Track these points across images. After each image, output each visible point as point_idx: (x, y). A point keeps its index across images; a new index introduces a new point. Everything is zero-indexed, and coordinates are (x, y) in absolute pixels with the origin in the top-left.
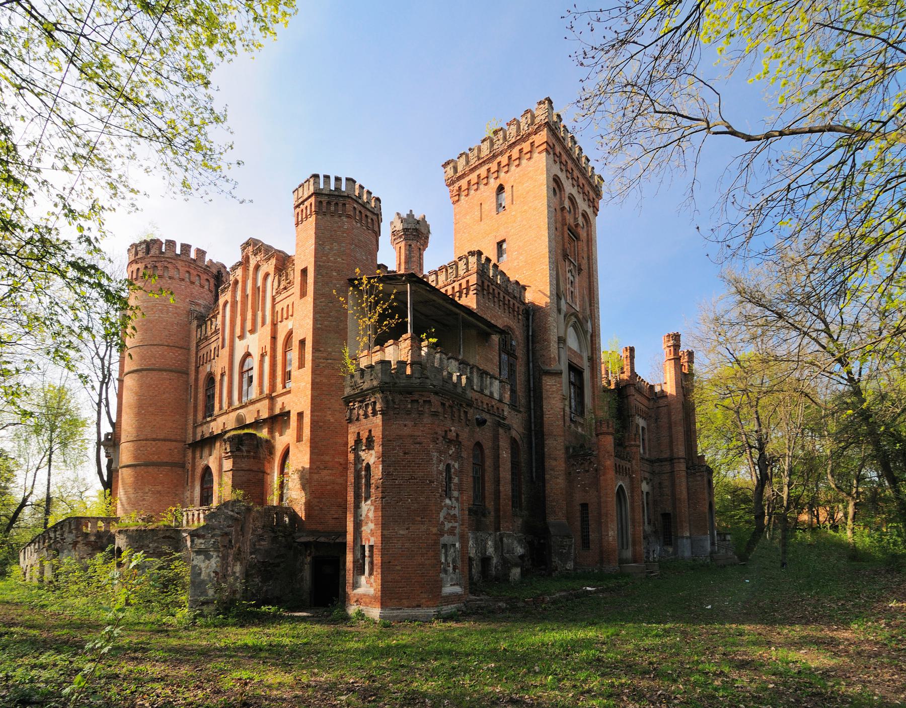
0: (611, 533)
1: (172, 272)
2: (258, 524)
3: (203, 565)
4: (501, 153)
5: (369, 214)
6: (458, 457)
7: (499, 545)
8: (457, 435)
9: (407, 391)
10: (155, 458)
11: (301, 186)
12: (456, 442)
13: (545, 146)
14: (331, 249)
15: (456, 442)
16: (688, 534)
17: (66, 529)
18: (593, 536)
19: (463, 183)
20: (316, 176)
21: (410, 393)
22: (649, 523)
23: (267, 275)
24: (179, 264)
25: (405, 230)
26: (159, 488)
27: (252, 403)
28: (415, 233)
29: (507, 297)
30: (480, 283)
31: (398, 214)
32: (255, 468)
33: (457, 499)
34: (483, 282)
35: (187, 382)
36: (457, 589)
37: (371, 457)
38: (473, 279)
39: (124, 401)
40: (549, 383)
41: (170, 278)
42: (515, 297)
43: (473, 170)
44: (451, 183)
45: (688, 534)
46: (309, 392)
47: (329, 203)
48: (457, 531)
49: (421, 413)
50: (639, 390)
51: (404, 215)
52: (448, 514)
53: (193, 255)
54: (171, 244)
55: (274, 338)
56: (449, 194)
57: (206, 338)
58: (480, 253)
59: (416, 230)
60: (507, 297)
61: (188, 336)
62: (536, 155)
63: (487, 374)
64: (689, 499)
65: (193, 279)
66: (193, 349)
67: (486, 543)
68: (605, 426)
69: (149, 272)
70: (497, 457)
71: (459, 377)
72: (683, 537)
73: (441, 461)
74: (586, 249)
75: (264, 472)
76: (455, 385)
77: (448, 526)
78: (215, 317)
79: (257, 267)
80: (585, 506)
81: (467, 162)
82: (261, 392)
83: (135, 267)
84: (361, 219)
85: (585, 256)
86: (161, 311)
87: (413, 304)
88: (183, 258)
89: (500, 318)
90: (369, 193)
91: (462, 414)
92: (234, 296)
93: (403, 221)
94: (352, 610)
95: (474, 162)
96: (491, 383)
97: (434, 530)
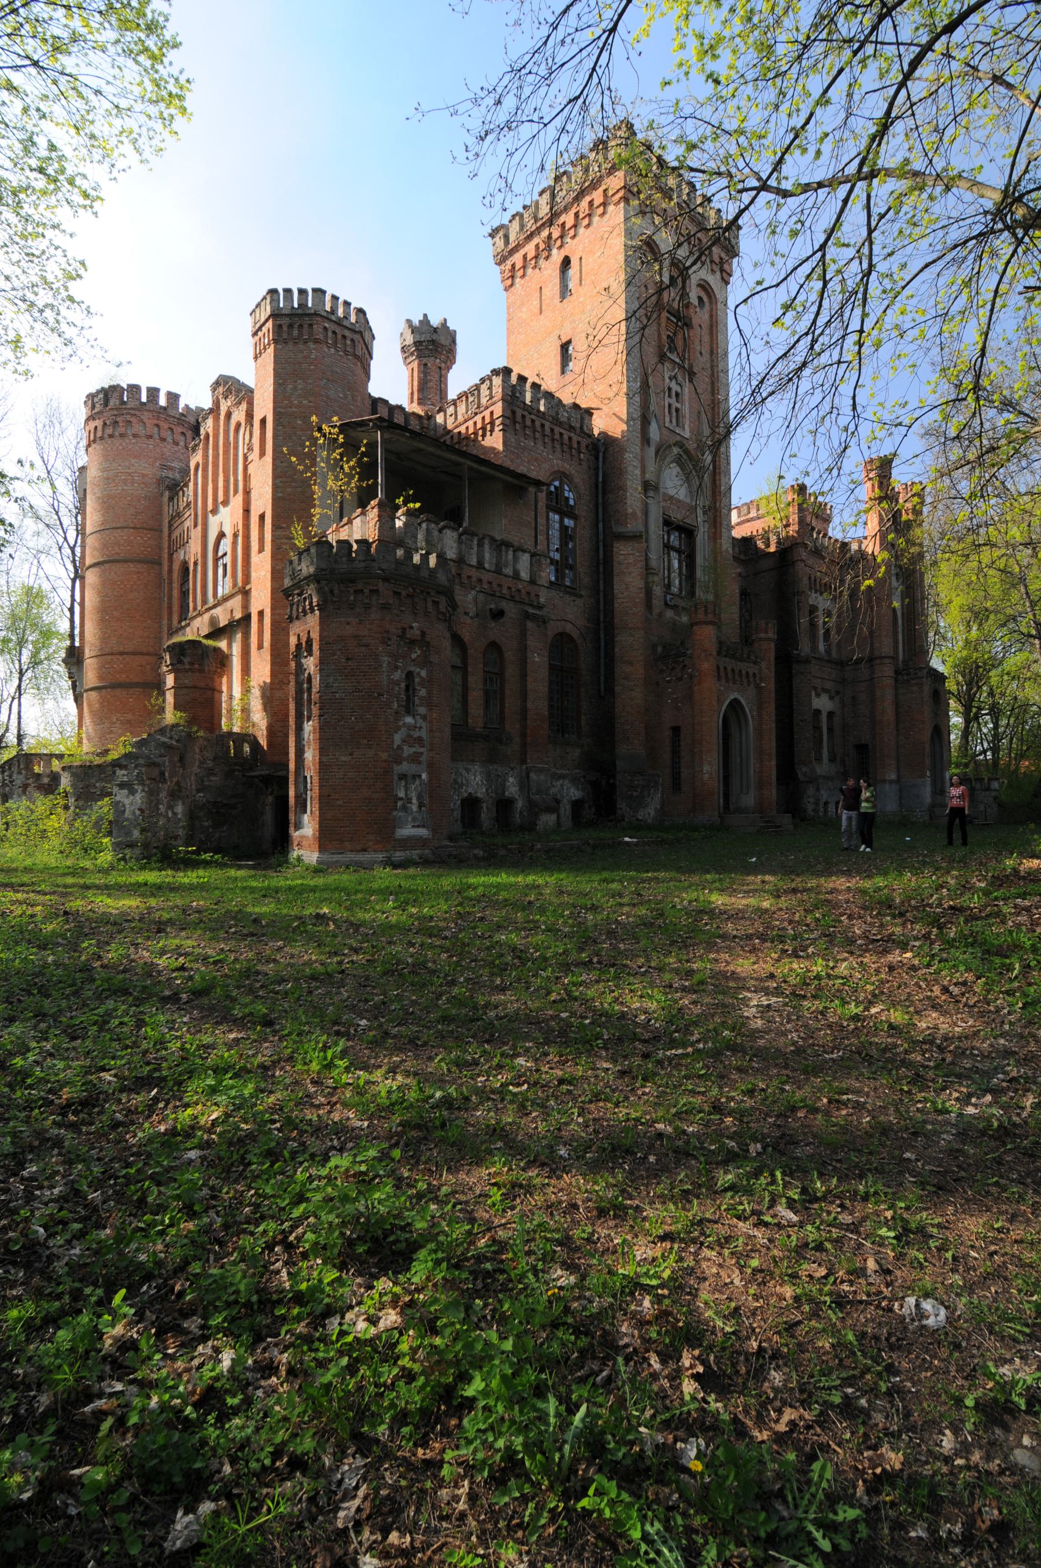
0: (706, 768)
1: (137, 428)
2: (209, 755)
3: (127, 802)
4: (566, 209)
5: (347, 333)
6: (424, 661)
7: (524, 783)
8: (423, 634)
9: (349, 579)
10: (123, 678)
11: (258, 305)
12: (422, 641)
13: (621, 193)
14: (295, 389)
15: (422, 641)
16: (893, 777)
17: (15, 769)
18: (685, 773)
19: (517, 258)
20: (273, 292)
21: (352, 581)
22: (832, 759)
23: (238, 425)
24: (145, 416)
25: (417, 344)
26: (129, 716)
27: (226, 599)
28: (432, 347)
29: (557, 430)
30: (509, 414)
31: (409, 321)
32: (202, 684)
33: (424, 718)
34: (514, 412)
35: (160, 574)
36: (423, 832)
37: (311, 664)
38: (498, 409)
39: (699, 560)
40: (625, 554)
41: (135, 436)
42: (571, 428)
43: (530, 237)
44: (501, 259)
45: (893, 777)
46: (269, 584)
47: (291, 326)
48: (423, 758)
49: (367, 607)
50: (817, 552)
51: (416, 322)
52: (409, 736)
53: (163, 402)
54: (134, 389)
55: (247, 511)
56: (499, 277)
57: (179, 515)
58: (507, 371)
59: (433, 342)
60: (557, 430)
61: (160, 513)
62: (611, 208)
63: (508, 545)
64: (898, 722)
65: (163, 434)
66: (166, 530)
67: (505, 780)
68: (701, 611)
69: (109, 431)
70: (523, 662)
71: (425, 558)
72: (884, 781)
73: (397, 668)
74: (706, 339)
75: (213, 690)
76: (417, 567)
77: (407, 751)
78: (186, 485)
79: (229, 415)
80: (676, 730)
81: (522, 226)
82: (235, 585)
83: (92, 425)
84: (335, 342)
85: (706, 350)
86: (125, 482)
87: (386, 460)
88: (150, 406)
89: (541, 463)
90: (347, 304)
91: (430, 605)
92: (205, 456)
93: (414, 330)
94: (295, 854)
95: (530, 225)
96: (516, 559)
97: (384, 756)
